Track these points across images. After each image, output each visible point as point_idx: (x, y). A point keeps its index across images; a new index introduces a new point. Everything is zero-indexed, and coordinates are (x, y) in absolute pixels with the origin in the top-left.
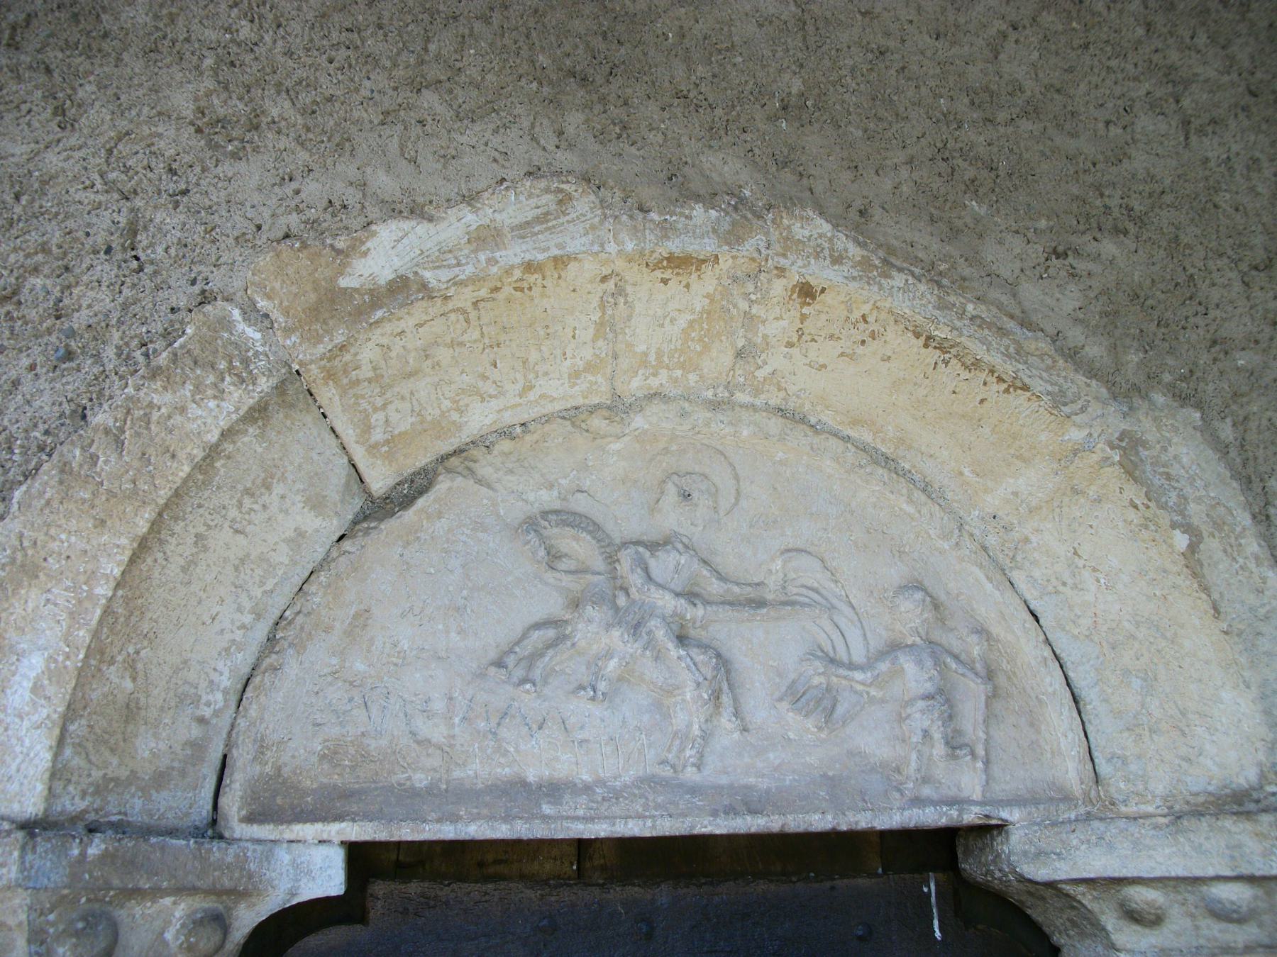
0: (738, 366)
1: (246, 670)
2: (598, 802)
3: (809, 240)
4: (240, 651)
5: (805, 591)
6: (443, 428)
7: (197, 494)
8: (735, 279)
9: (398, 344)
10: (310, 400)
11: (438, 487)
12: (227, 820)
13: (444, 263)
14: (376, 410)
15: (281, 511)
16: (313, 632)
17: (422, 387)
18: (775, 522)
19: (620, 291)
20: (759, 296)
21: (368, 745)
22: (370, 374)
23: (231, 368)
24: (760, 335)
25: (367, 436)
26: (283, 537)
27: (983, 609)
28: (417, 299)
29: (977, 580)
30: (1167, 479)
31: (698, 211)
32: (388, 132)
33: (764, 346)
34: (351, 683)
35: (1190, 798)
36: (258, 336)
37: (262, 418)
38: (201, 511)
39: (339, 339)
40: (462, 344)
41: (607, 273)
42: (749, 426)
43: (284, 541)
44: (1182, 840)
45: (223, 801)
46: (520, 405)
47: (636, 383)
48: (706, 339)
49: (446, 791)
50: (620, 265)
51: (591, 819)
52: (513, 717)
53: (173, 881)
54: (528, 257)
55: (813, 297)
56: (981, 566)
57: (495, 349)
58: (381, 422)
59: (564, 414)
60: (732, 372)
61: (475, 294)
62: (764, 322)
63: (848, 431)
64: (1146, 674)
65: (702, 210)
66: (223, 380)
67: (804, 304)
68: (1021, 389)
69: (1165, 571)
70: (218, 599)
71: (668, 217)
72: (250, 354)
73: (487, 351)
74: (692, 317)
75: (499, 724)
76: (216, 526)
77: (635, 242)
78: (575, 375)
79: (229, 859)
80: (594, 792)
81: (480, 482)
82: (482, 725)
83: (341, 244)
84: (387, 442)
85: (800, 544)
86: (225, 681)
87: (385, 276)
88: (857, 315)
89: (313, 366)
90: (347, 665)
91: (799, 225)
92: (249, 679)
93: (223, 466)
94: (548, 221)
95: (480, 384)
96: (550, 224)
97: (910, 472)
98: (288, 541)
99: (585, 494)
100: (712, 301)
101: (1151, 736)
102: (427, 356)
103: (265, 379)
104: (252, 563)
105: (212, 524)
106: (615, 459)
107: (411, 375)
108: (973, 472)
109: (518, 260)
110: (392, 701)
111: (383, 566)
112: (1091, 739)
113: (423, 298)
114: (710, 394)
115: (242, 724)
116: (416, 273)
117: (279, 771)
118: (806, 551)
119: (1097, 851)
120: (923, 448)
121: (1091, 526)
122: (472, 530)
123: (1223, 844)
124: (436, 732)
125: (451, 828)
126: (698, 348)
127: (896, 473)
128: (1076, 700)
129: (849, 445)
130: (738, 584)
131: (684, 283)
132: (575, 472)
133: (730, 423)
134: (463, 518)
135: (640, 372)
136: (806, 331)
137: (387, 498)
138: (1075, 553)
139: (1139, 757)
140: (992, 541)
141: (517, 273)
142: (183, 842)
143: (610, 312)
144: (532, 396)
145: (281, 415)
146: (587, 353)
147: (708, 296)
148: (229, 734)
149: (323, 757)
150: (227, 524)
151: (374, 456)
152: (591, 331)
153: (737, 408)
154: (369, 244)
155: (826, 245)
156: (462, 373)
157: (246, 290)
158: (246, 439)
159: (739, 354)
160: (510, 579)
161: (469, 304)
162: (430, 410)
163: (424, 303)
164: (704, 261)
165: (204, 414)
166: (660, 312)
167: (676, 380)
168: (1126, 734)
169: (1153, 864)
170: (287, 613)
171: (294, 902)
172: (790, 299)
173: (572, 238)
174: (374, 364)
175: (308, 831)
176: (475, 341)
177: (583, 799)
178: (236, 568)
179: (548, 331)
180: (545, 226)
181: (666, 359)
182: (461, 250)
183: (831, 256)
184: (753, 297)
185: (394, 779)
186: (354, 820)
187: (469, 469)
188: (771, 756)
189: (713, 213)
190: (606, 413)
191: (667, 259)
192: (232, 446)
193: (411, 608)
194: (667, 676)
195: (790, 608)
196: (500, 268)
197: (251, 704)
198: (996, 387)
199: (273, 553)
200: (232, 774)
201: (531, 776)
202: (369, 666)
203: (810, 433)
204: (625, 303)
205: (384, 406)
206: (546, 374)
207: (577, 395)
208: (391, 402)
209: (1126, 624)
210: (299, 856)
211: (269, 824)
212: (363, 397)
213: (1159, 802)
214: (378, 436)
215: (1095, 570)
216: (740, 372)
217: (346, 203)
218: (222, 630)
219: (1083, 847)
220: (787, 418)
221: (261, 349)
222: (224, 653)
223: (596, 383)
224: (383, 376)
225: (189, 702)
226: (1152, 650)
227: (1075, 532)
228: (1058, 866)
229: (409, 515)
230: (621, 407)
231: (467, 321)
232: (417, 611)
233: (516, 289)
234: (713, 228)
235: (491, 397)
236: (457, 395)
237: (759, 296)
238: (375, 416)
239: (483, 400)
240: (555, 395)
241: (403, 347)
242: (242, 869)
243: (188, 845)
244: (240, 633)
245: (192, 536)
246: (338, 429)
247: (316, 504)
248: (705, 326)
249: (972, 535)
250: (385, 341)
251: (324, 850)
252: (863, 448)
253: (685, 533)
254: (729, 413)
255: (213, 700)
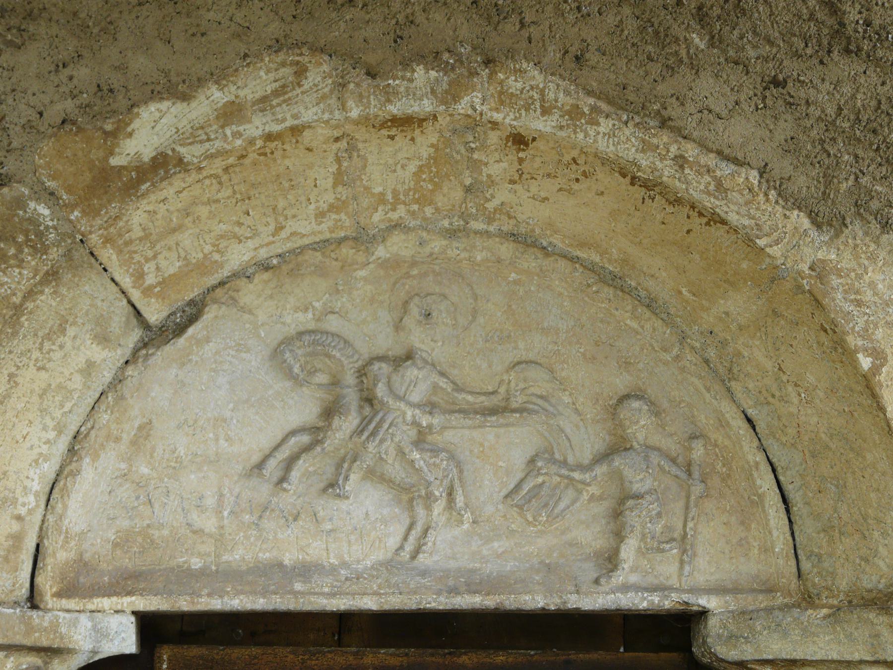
0: (468, 199)
1: (53, 476)
2: (341, 582)
3: (522, 92)
4: (45, 461)
5: (534, 399)
6: (207, 267)
7: (7, 343)
8: (454, 131)
9: (162, 209)
10: (93, 260)
11: (205, 317)
12: (41, 595)
13: (197, 139)
14: (147, 260)
15: (74, 348)
16: (105, 443)
17: (186, 239)
18: (509, 337)
19: (352, 148)
20: (478, 144)
21: (153, 535)
22: (141, 234)
23: (28, 240)
24: (484, 174)
25: (141, 282)
26: (77, 368)
27: (703, 416)
28: (175, 173)
29: (696, 390)
30: (856, 306)
31: (420, 72)
32: (145, 13)
33: (490, 183)
34: (138, 484)
35: (865, 594)
36: (46, 212)
37: (55, 280)
38: (11, 356)
39: (113, 212)
40: (217, 201)
41: (339, 135)
42: (482, 251)
43: (77, 371)
44: (838, 629)
45: (39, 580)
46: (273, 242)
47: (377, 217)
48: (436, 180)
49: (217, 571)
50: (349, 128)
51: (332, 595)
52: (273, 510)
53: (6, 639)
54: (267, 129)
55: (527, 145)
56: (700, 377)
57: (247, 201)
58: (153, 269)
59: (315, 246)
60: (464, 205)
61: (224, 163)
62: (486, 164)
63: (578, 253)
64: (838, 481)
65: (423, 72)
66: (21, 252)
67: (520, 150)
68: (720, 223)
69: (851, 390)
70: (27, 422)
71: (391, 82)
72: (42, 228)
73: (239, 204)
74: (420, 163)
75: (260, 517)
76: (24, 366)
77: (361, 108)
78: (320, 215)
79: (46, 624)
80: (339, 573)
81: (242, 309)
82: (247, 517)
83: (109, 127)
84: (159, 283)
85: (531, 356)
86: (36, 486)
87: (147, 154)
88: (567, 158)
89: (93, 236)
90: (134, 469)
91: (513, 78)
92: (54, 483)
93: (26, 320)
94: (286, 93)
95: (237, 229)
96: (286, 97)
97: (636, 289)
98: (80, 371)
99: (336, 315)
100: (437, 150)
101: (840, 538)
102: (188, 215)
103: (55, 249)
104: (53, 391)
105: (20, 364)
106: (362, 283)
107: (174, 231)
108: (690, 292)
109: (259, 132)
110: (171, 498)
111: (161, 385)
112: (797, 538)
113: (180, 172)
114: (446, 223)
115: (51, 520)
116: (173, 150)
117: (81, 556)
118: (536, 363)
119: (776, 636)
120: (645, 269)
121: (791, 345)
122: (237, 351)
123: (867, 634)
124: (209, 524)
125: (219, 601)
126: (430, 187)
127: (622, 291)
128: (785, 500)
129: (577, 266)
130: (471, 393)
131: (409, 137)
132: (327, 295)
133: (465, 249)
134: (228, 341)
135: (380, 208)
136: (525, 171)
137: (163, 326)
138: (780, 369)
139: (830, 555)
140: (712, 353)
141: (259, 143)
142: (12, 611)
143: (345, 164)
144: (284, 234)
145: (70, 276)
146: (330, 197)
147: (432, 146)
148: (41, 529)
149: (116, 545)
150: (32, 363)
151: (149, 296)
152: (330, 180)
153: (472, 235)
154: (132, 126)
155: (536, 96)
156: (219, 223)
157: (35, 173)
158: (43, 298)
159: (468, 190)
160: (270, 392)
161: (220, 171)
162: (194, 255)
163: (181, 175)
164: (424, 120)
165: (9, 281)
166: (391, 161)
167: (413, 214)
168: (822, 535)
169: (817, 649)
170: (83, 429)
171: (96, 658)
172: (506, 146)
173: (306, 108)
174: (143, 226)
175: (106, 603)
176: (228, 198)
177: (329, 580)
178: (41, 396)
179: (292, 183)
180: (282, 98)
181: (402, 197)
182: (210, 126)
183: (542, 106)
184: (473, 145)
185: (173, 563)
186: (141, 595)
187: (232, 298)
188: (496, 544)
189: (433, 74)
190: (351, 243)
191: (390, 120)
192: (33, 304)
193: (186, 420)
194: (403, 476)
195: (518, 415)
196: (244, 140)
197: (57, 503)
198: (697, 221)
199: (68, 382)
200: (44, 559)
201: (287, 560)
202: (152, 470)
203: (540, 256)
204: (358, 156)
205: (155, 257)
206: (294, 216)
207: (324, 229)
208: (160, 253)
209: (823, 436)
210: (100, 623)
211: (75, 598)
212: (135, 252)
213: (842, 597)
214: (150, 280)
215: (796, 385)
216: (471, 204)
217: (112, 87)
218: (32, 446)
219: (765, 632)
220: (519, 242)
221: (50, 224)
222: (33, 464)
223: (340, 220)
224: (151, 234)
225: (9, 503)
226: (843, 461)
227: (778, 350)
228: (745, 648)
229: (182, 341)
230: (365, 238)
231: (220, 183)
232: (191, 423)
233: (260, 155)
234: (432, 89)
235: (247, 238)
236: (217, 240)
237: (478, 144)
238: (147, 265)
239: (240, 242)
240: (304, 232)
241: (167, 210)
242: (56, 632)
243: (15, 613)
244: (45, 447)
245: (6, 376)
246: (117, 278)
247: (103, 339)
248: (434, 169)
249: (693, 348)
250: (150, 208)
251: (118, 618)
252: (591, 268)
253: (426, 349)
254: (464, 240)
255: (27, 501)
